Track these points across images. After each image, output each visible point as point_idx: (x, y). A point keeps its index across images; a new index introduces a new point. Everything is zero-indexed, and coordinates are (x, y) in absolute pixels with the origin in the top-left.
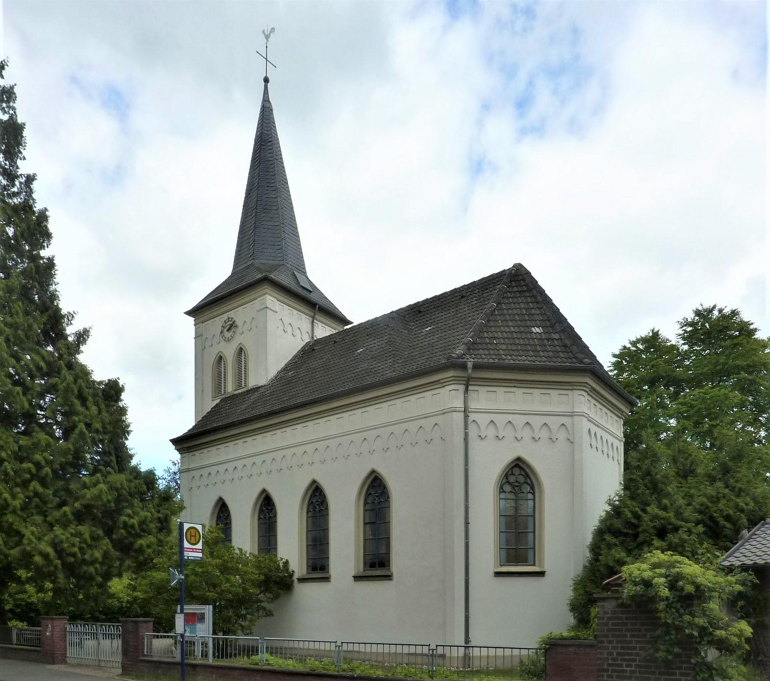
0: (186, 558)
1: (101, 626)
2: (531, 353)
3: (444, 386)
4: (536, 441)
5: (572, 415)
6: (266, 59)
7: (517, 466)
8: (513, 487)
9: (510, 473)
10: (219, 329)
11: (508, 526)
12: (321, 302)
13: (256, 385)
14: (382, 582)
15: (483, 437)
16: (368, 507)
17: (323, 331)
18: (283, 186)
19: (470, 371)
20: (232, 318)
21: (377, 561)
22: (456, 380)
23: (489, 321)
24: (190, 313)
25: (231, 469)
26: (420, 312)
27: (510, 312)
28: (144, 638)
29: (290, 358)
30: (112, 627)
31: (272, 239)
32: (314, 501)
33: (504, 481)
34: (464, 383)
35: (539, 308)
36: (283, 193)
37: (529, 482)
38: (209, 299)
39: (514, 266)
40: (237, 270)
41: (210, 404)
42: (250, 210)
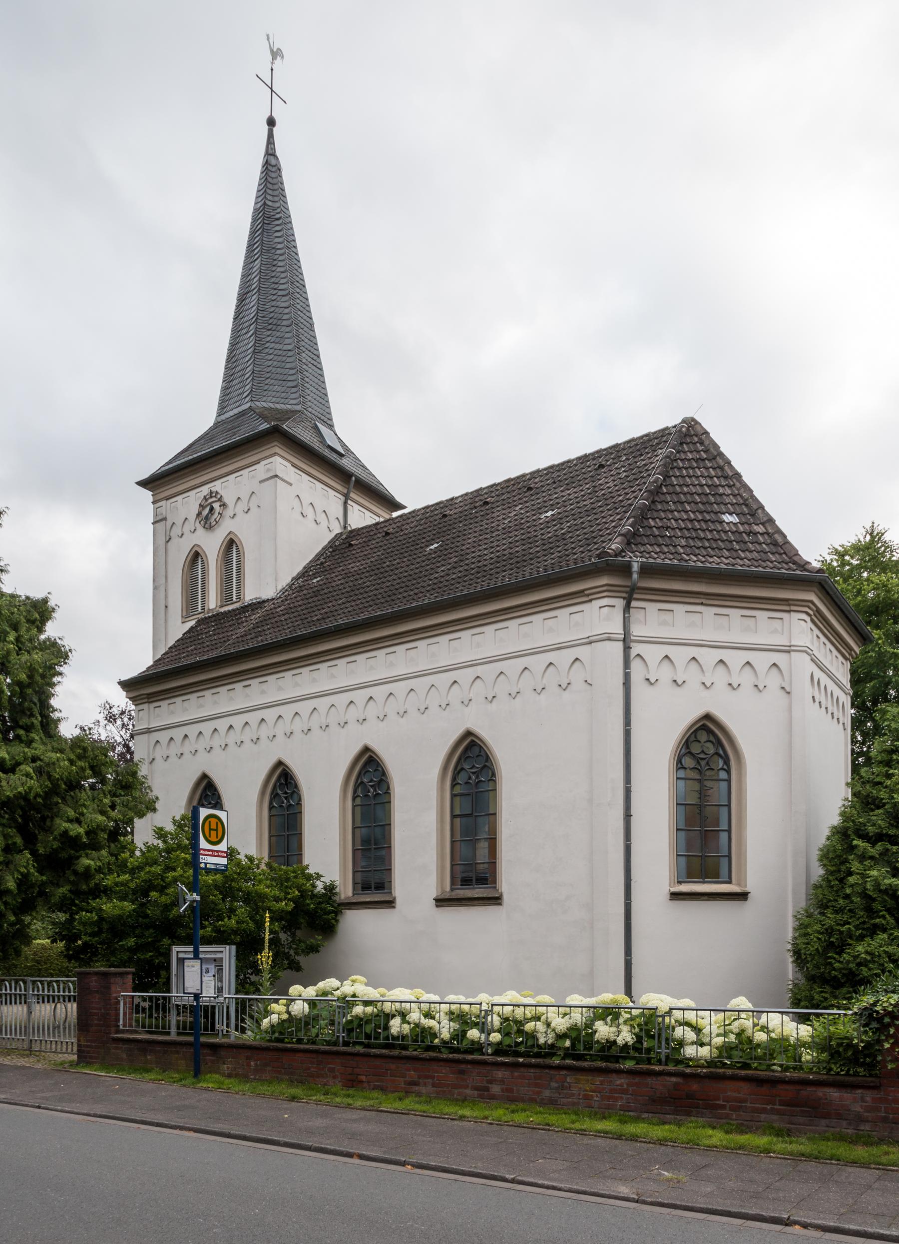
0: (202, 865)
1: (17, 982)
2: (727, 553)
3: (590, 601)
4: (734, 689)
5: (787, 650)
6: (272, 90)
7: (704, 728)
8: (698, 761)
9: (693, 738)
10: (195, 509)
11: (689, 821)
12: (358, 472)
13: (256, 598)
14: (484, 908)
15: (653, 681)
16: (274, 812)
17: (362, 517)
18: (298, 290)
19: (635, 576)
20: (217, 493)
21: (473, 875)
22: (612, 591)
23: (653, 502)
24: (144, 484)
25: (254, 723)
26: (530, 489)
27: (685, 489)
28: (118, 1003)
29: (311, 557)
30: (55, 984)
31: (282, 371)
32: (467, 767)
33: (683, 751)
34: (624, 595)
35: (730, 486)
36: (298, 301)
37: (721, 752)
38: (178, 462)
39: (684, 421)
40: (223, 417)
41: (178, 629)
42: (247, 324)
